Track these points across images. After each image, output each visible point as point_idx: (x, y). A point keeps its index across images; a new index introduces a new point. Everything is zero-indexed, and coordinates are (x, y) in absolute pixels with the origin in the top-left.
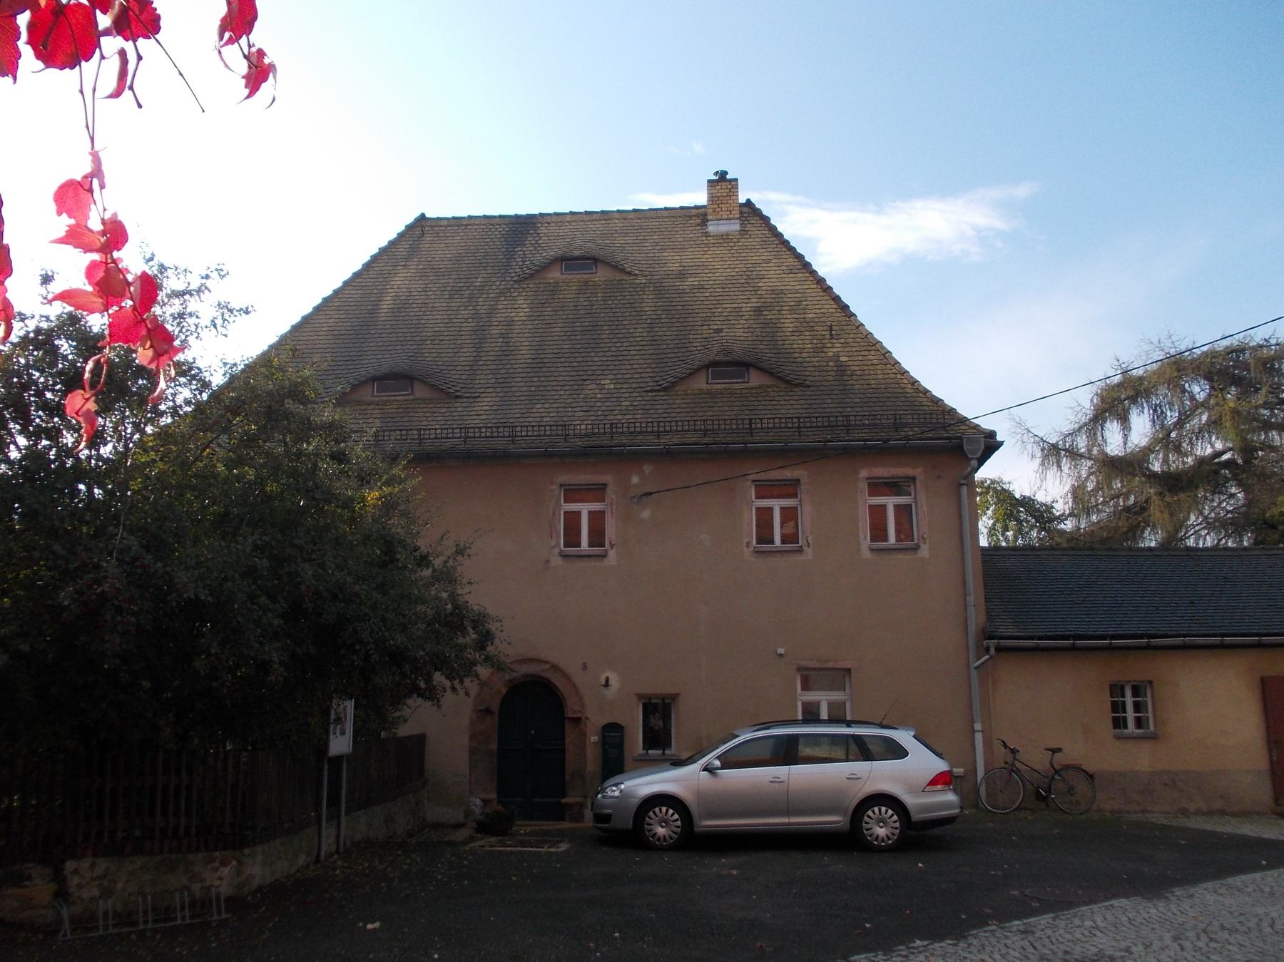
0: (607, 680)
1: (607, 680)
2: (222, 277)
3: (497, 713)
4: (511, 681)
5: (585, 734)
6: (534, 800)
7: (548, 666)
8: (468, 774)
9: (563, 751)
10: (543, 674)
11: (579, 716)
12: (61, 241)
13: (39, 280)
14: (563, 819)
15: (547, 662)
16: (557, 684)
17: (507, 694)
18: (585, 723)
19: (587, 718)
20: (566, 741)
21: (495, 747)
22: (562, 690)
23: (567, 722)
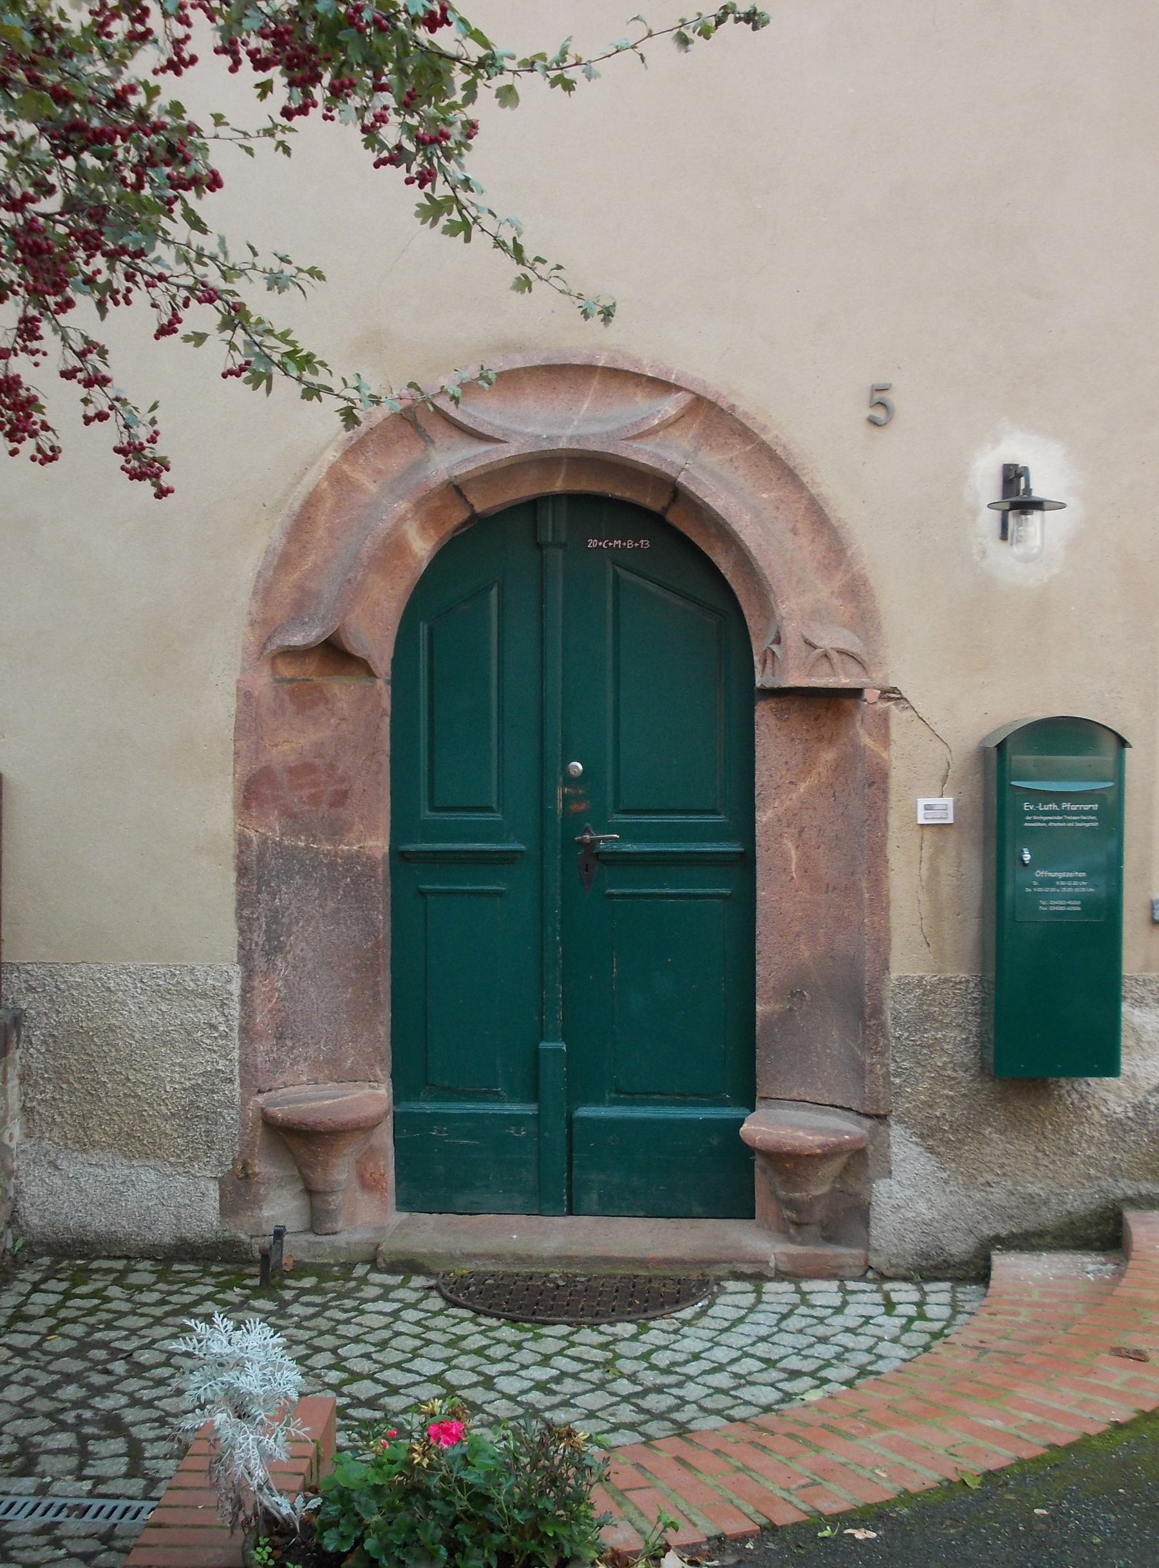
0: (1012, 476)
1: (1012, 476)
2: (325, 117)
3: (383, 664)
4: (456, 489)
5: (878, 779)
6: (584, 1112)
7: (670, 406)
8: (235, 987)
9: (746, 861)
10: (644, 454)
11: (844, 681)
12: (212, 115)
13: (223, 176)
14: (746, 1212)
15: (662, 386)
16: (719, 501)
17: (442, 557)
18: (884, 719)
19: (890, 694)
20: (763, 817)
21: (379, 845)
22: (754, 552)
23: (764, 716)
